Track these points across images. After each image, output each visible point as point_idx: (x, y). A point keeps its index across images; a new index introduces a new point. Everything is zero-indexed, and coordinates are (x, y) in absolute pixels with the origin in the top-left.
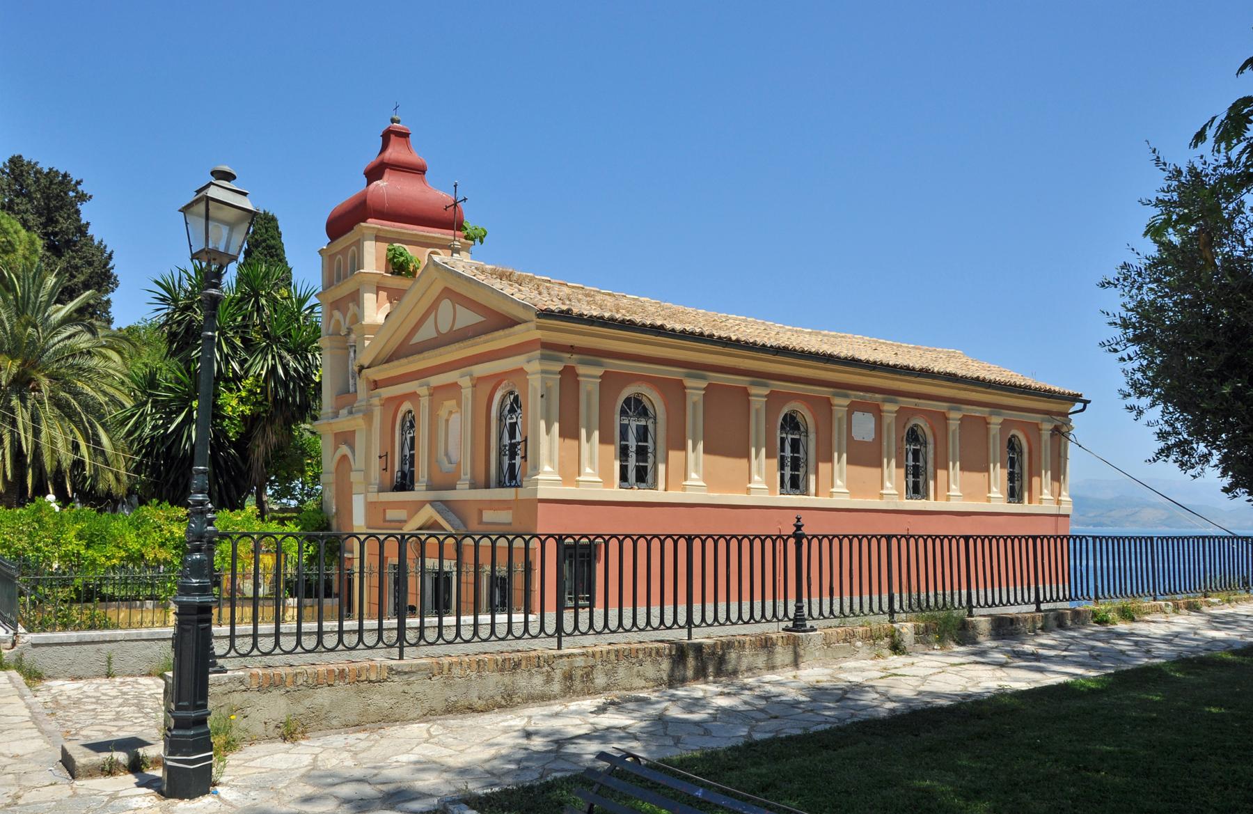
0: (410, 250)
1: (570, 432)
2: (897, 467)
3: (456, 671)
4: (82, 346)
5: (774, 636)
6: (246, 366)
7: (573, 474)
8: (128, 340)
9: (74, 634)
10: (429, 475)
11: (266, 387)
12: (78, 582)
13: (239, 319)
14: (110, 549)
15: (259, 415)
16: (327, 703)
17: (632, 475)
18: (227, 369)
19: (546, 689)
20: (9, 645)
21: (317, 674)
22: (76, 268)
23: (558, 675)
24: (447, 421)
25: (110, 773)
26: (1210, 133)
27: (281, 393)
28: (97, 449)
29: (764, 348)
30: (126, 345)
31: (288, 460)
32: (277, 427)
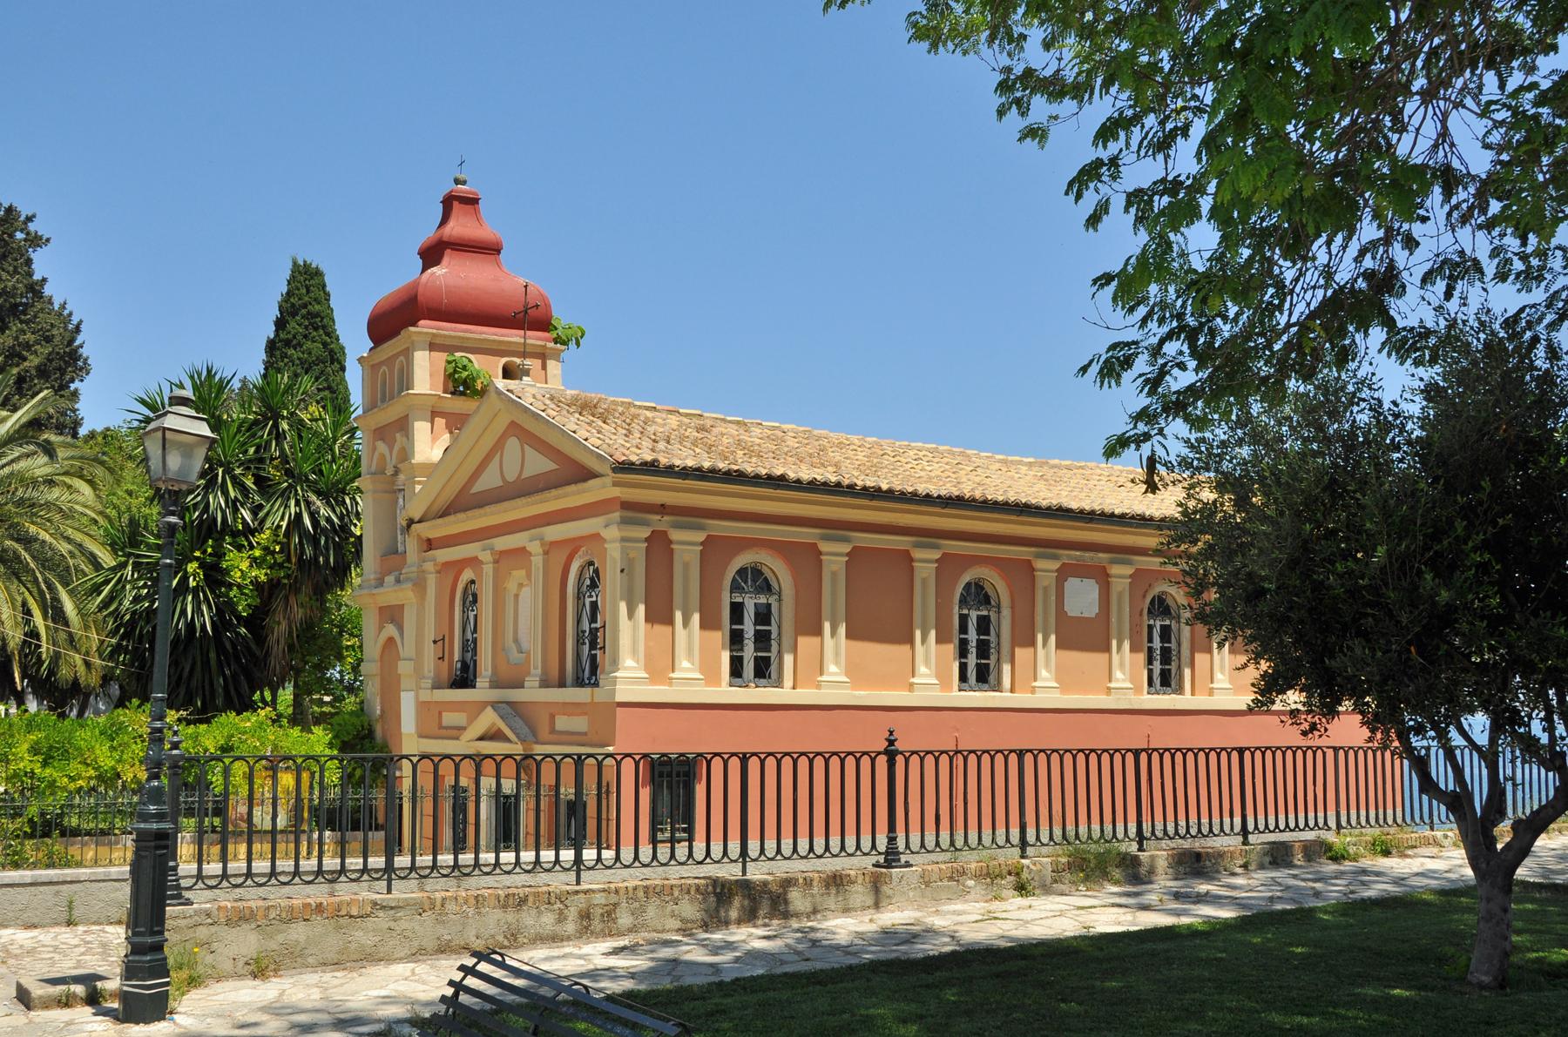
0: (478, 363)
1: (660, 614)
2: (1132, 650)
3: (451, 906)
4: (38, 472)
5: (852, 873)
6: (261, 514)
7: (665, 670)
8: (102, 463)
9: (28, 873)
10: (494, 667)
11: (289, 544)
12: (33, 810)
13: (252, 450)
14: (75, 767)
15: (279, 581)
16: (302, 938)
17: (749, 668)
18: (235, 520)
19: (558, 928)
21: (291, 908)
22: (28, 346)
23: (572, 913)
24: (517, 596)
25: (67, 1005)
26: (1095, 368)
27: (309, 551)
28: (56, 614)
29: (928, 499)
30: (99, 471)
31: (320, 642)
32: (303, 598)
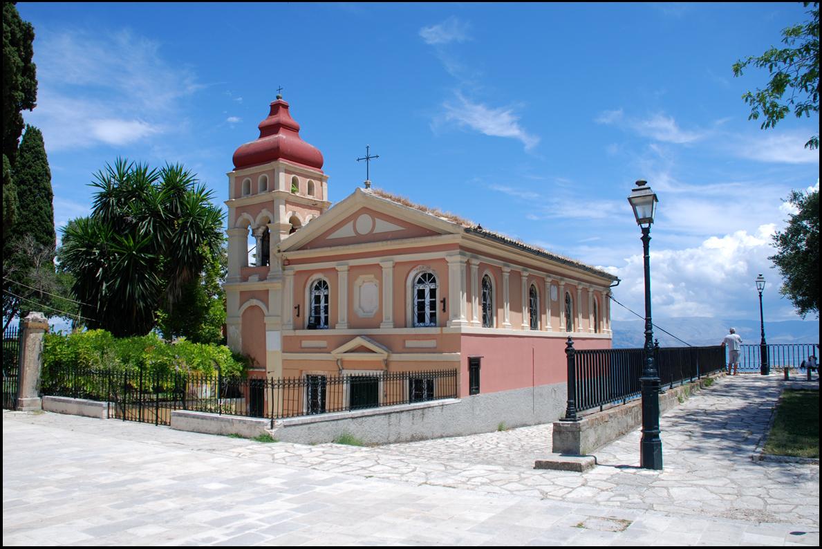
10: (348, 319)
20: (269, 427)
